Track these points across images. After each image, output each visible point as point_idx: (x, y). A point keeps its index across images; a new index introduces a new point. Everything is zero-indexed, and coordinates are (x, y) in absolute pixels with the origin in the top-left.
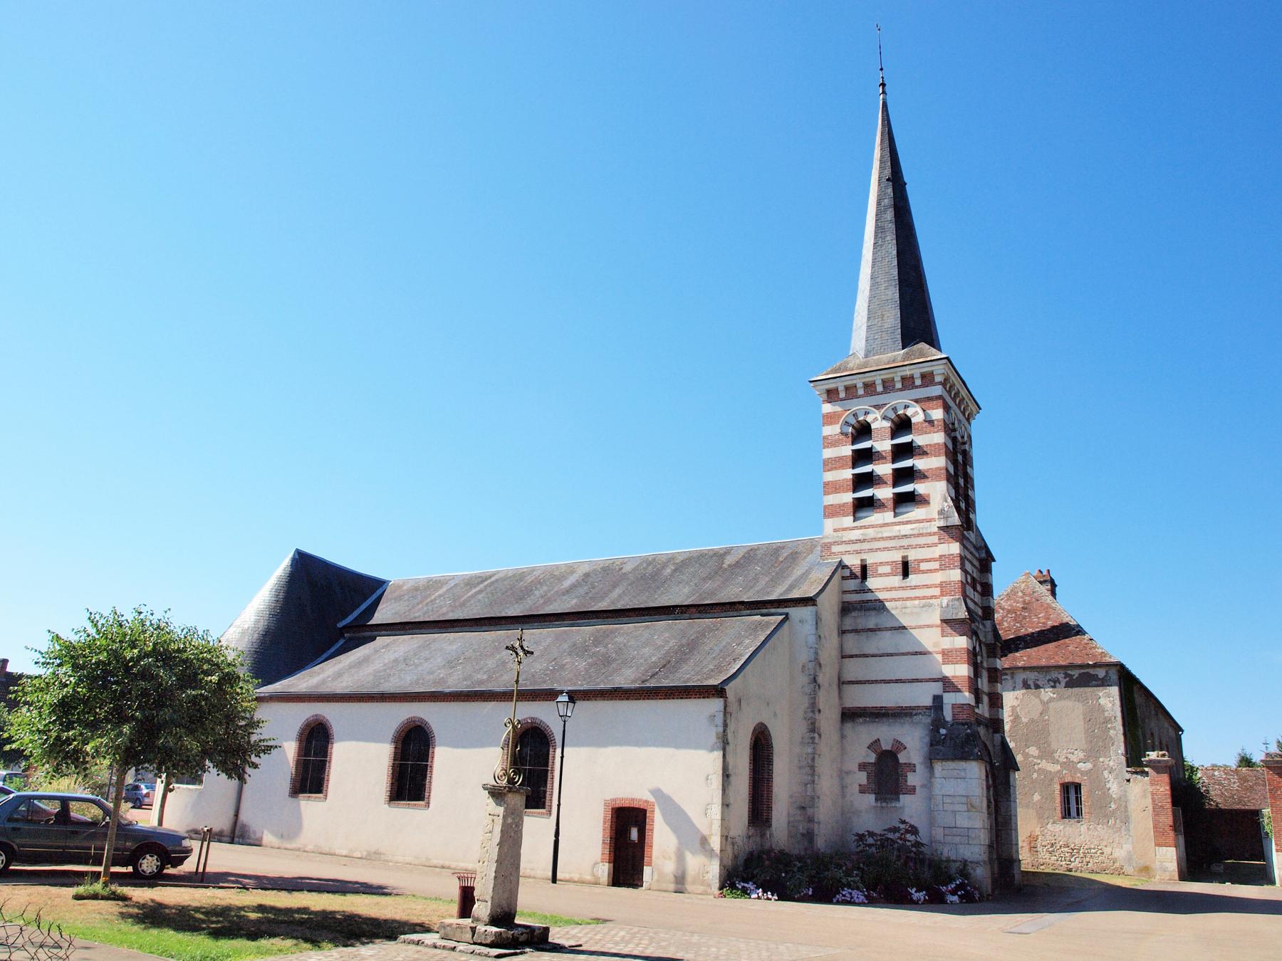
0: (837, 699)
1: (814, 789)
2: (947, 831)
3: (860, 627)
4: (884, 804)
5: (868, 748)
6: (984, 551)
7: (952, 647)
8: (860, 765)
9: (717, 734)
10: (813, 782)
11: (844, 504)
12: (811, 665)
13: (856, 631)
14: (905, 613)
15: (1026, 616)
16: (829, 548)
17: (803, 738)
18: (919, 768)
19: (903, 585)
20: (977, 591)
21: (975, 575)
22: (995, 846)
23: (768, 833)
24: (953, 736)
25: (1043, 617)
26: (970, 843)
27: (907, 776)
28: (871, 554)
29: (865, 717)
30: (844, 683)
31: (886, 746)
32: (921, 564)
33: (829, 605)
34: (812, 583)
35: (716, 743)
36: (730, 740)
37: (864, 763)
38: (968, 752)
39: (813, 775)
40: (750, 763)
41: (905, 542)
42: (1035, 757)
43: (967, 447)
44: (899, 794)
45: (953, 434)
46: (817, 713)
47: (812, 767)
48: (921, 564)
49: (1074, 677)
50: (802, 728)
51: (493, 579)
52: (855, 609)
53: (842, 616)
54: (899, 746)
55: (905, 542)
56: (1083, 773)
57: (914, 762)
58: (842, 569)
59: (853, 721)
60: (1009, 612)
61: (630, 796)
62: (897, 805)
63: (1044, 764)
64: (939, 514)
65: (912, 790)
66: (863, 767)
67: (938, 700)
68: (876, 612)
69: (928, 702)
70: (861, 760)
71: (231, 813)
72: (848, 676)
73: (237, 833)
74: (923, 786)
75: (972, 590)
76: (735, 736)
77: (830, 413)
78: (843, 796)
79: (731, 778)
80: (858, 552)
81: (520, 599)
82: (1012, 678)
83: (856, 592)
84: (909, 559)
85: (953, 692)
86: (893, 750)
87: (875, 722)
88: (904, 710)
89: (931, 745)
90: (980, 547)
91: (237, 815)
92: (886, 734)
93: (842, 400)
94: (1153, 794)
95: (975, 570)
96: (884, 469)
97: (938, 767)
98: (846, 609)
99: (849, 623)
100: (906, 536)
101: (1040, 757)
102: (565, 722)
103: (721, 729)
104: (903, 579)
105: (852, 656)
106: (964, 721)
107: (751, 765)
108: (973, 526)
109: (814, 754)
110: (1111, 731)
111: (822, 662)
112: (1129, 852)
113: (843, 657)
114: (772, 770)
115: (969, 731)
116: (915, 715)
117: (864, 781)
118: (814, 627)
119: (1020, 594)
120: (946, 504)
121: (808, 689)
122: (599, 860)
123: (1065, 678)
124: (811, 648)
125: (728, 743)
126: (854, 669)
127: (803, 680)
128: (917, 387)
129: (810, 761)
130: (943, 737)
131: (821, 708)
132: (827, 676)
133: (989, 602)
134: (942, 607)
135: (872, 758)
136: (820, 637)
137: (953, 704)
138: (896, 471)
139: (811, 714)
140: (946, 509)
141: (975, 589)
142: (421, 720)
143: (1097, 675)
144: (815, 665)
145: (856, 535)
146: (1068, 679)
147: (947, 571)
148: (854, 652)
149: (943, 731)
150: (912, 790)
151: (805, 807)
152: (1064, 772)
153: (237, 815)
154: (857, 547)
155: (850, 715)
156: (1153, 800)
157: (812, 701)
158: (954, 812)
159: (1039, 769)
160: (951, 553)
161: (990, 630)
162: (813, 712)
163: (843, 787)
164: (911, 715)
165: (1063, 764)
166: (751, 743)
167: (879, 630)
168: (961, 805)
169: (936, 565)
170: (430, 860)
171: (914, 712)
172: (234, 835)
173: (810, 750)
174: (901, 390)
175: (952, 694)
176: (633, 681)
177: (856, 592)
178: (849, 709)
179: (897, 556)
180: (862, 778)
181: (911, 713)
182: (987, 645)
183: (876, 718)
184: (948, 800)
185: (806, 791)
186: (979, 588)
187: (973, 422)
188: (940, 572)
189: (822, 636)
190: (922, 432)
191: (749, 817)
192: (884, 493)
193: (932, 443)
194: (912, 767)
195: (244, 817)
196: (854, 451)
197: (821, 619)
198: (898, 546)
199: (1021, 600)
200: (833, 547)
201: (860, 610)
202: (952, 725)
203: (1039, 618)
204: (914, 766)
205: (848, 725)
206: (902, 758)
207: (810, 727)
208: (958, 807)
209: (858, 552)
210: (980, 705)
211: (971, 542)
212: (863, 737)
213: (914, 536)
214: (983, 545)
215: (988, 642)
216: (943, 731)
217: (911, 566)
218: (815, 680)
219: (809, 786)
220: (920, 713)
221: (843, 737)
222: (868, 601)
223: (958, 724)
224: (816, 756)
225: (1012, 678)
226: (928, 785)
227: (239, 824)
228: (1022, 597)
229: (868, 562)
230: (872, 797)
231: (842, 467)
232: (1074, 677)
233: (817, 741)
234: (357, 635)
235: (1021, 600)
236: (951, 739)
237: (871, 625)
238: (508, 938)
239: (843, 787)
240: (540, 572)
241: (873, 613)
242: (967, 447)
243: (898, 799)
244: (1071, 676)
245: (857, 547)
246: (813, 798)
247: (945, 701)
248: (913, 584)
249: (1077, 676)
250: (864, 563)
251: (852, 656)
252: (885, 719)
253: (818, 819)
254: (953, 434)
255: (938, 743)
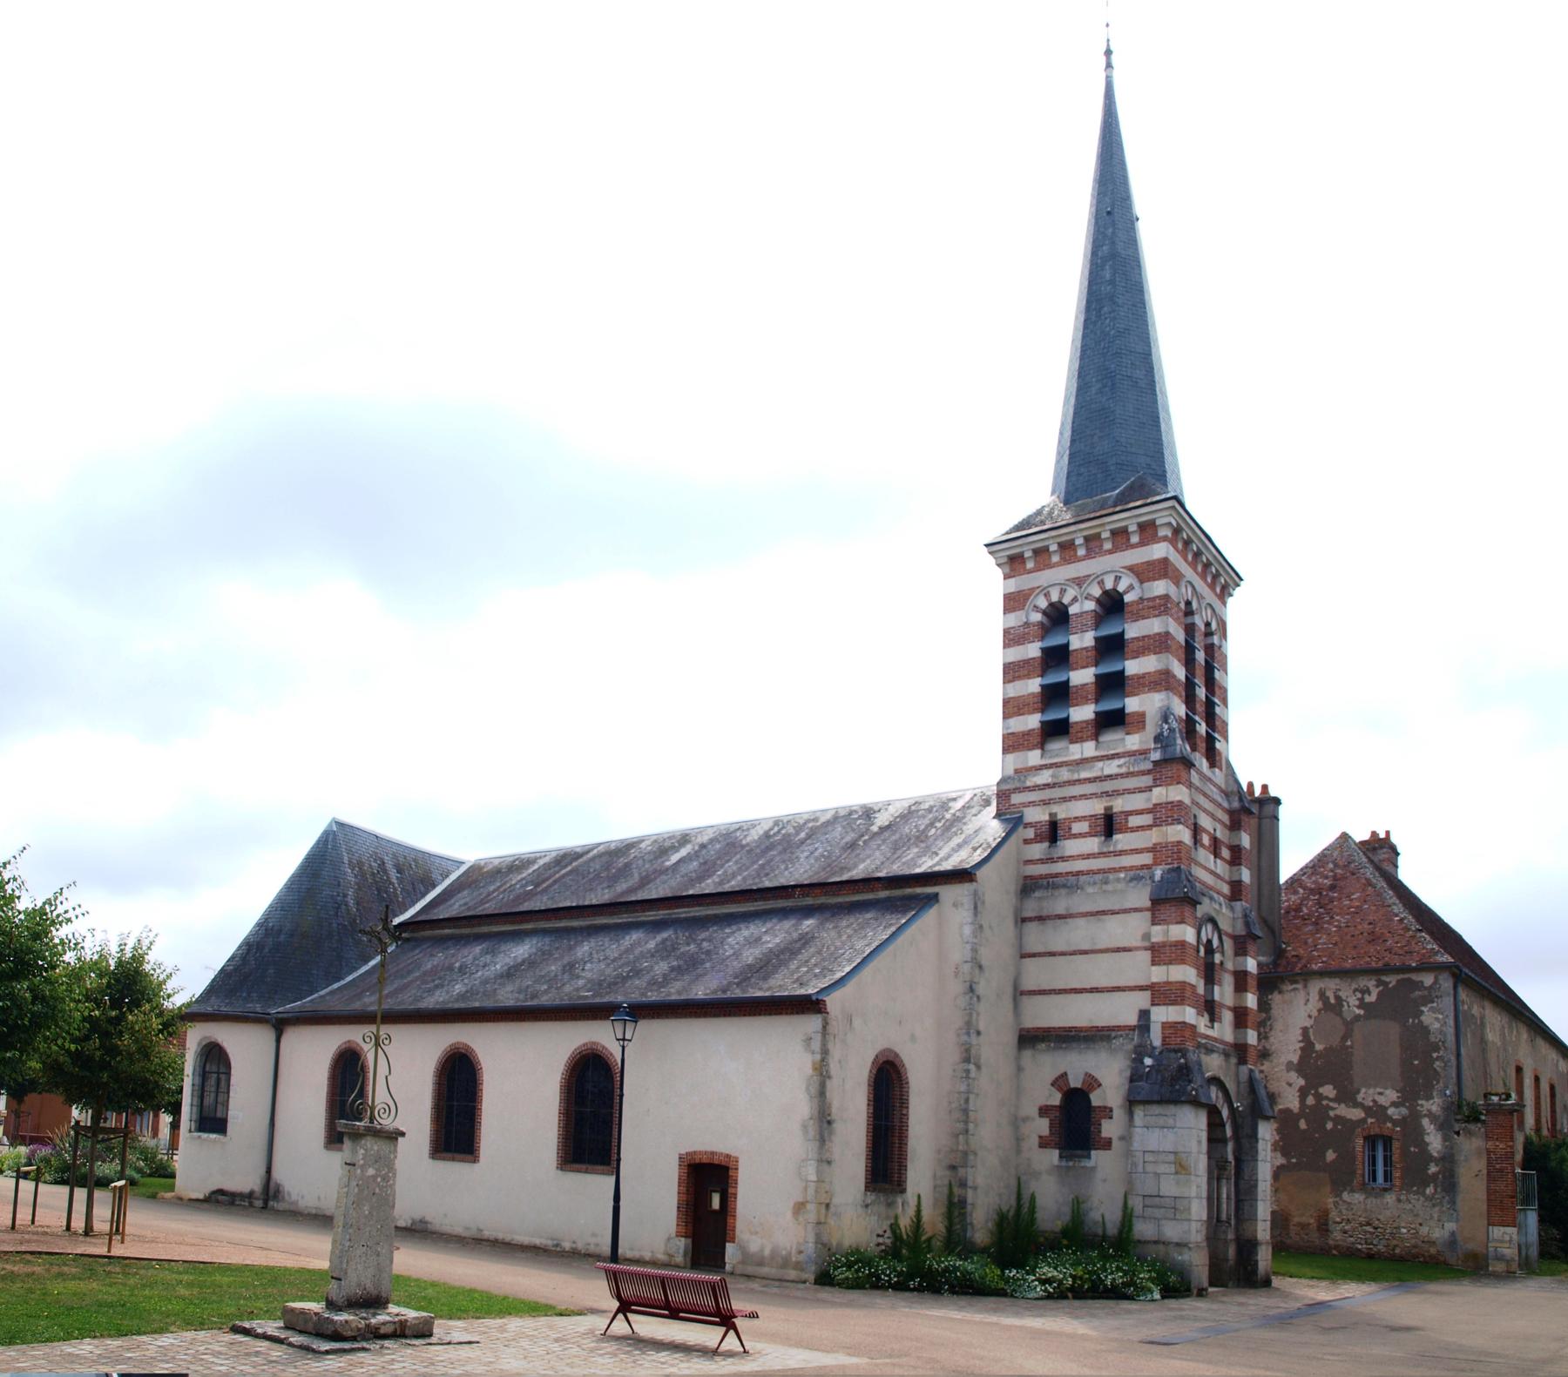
0: (1010, 1015)
1: (967, 1142)
2: (1148, 1201)
3: (1045, 913)
4: (1071, 1164)
5: (1052, 1085)
6: (1237, 798)
7: (1165, 939)
8: (1041, 1109)
9: (814, 1063)
10: (967, 1131)
11: (1030, 731)
12: (966, 968)
13: (1041, 919)
14: (1105, 891)
15: (1334, 897)
16: (1008, 797)
17: (954, 1071)
18: (1118, 1113)
19: (1105, 850)
20: (1223, 859)
21: (1218, 834)
22: (1233, 1222)
23: (900, 1201)
24: (1162, 1068)
25: (1358, 899)
26: (1177, 1217)
27: (1100, 1125)
28: (1064, 806)
29: (1049, 1041)
30: (1023, 993)
31: (1075, 1082)
32: (1130, 818)
33: (997, 885)
34: (975, 849)
35: (812, 1076)
36: (833, 1073)
37: (1047, 1106)
38: (1178, 1091)
39: (966, 1122)
40: (868, 1105)
41: (1108, 786)
42: (1331, 1100)
43: (1216, 639)
44: (1059, 1148)
45: (1189, 620)
46: (973, 1036)
47: (965, 1111)
48: (1130, 818)
49: (1390, 986)
50: (954, 1055)
51: (591, 854)
52: (1040, 887)
53: (1022, 899)
54: (1092, 1083)
55: (1108, 786)
56: (1395, 1123)
57: (1109, 1105)
58: (1025, 828)
59: (1034, 1047)
60: (1312, 891)
61: (709, 1148)
62: (1088, 1165)
63: (1343, 1110)
64: (1155, 742)
65: (1107, 1144)
66: (1044, 1111)
67: (1144, 1015)
68: (1067, 890)
69: (1132, 1020)
70: (1043, 1102)
71: (262, 1171)
72: (1029, 983)
73: (271, 1192)
74: (1122, 1138)
75: (1212, 857)
76: (841, 1067)
77: (1013, 593)
78: (1018, 1151)
79: (834, 1125)
80: (1046, 803)
81: (614, 879)
82: (1305, 987)
83: (1042, 861)
84: (1115, 810)
85: (1164, 1004)
86: (1084, 1088)
87: (1061, 1048)
88: (1099, 1031)
89: (1132, 1080)
90: (1232, 792)
91: (269, 1171)
92: (1077, 1064)
93: (1030, 572)
94: (1489, 1152)
95: (1219, 827)
96: (1082, 677)
97: (1139, 1113)
98: (1028, 886)
99: (1030, 909)
100: (1110, 777)
101: (1338, 1100)
102: (623, 1047)
103: (818, 1057)
104: (1105, 840)
105: (1033, 955)
106: (1176, 1047)
107: (872, 1108)
108: (1221, 760)
109: (969, 1092)
110: (1438, 1063)
111: (983, 963)
112: (1453, 1234)
113: (1023, 956)
114: (907, 1115)
115: (1182, 1061)
116: (1114, 1038)
117: (1046, 1131)
118: (972, 911)
119: (1331, 866)
120: (1166, 727)
121: (963, 1002)
122: (674, 1235)
123: (1377, 986)
124: (967, 943)
125: (829, 1077)
126: (1036, 974)
127: (956, 987)
128: (1133, 546)
129: (962, 1102)
130: (1147, 1069)
131: (981, 1027)
132: (993, 984)
133: (1240, 874)
134: (1154, 882)
135: (1056, 1099)
136: (981, 927)
137: (1163, 1023)
138: (1100, 678)
139: (965, 1038)
140: (1165, 734)
141: (1216, 854)
142: (468, 1047)
143: (1422, 982)
144: (972, 968)
145: (1045, 777)
146: (1381, 988)
147: (1164, 828)
148: (1040, 949)
149: (1148, 1061)
150: (1107, 1144)
151: (956, 1166)
152: (1370, 1120)
153: (269, 1171)
154: (1046, 794)
155: (1029, 1039)
156: (1489, 1163)
157: (967, 1018)
158: (1157, 1175)
159: (1337, 1116)
160: (1170, 800)
161: (1240, 915)
162: (968, 1034)
163: (1019, 1140)
164: (1108, 1039)
165: (1368, 1110)
166: (870, 1076)
167: (1071, 916)
168: (1166, 1165)
169: (1146, 819)
170: (482, 1231)
171: (1113, 1034)
172: (267, 1194)
173: (963, 1088)
174: (1110, 552)
175: (1163, 1008)
176: (715, 992)
177: (1042, 861)
178: (1028, 1030)
179: (1097, 807)
180: (1043, 1126)
181: (1109, 1036)
182: (1235, 938)
183: (1064, 1042)
184: (1149, 1157)
185: (958, 1144)
186: (1226, 853)
187: (1230, 601)
188: (1154, 829)
189: (986, 926)
190: (1139, 616)
191: (866, 1179)
192: (1082, 713)
193: (1151, 633)
194: (1107, 1112)
195: (279, 1174)
196: (1043, 650)
197: (983, 903)
198: (1099, 792)
199: (1331, 874)
200: (1013, 795)
201: (1047, 887)
202: (1161, 1053)
203: (1351, 900)
204: (1111, 1110)
205: (1027, 1054)
206: (1096, 1099)
207: (964, 1055)
208: (1162, 1168)
209: (1046, 803)
210: (1216, 1025)
211: (1215, 785)
212: (1045, 1067)
213: (1121, 776)
214: (1235, 789)
215: (1237, 933)
216: (1148, 1061)
217: (1117, 819)
218: (971, 990)
219: (961, 1137)
220: (1121, 1036)
221: (1020, 1069)
222: (1057, 875)
223: (1170, 1051)
224: (972, 1097)
225: (1305, 987)
226: (1126, 1138)
227: (272, 1184)
228: (1332, 871)
229: (1059, 817)
230: (1056, 1153)
231: (1028, 676)
232: (1390, 986)
233: (973, 1075)
234: (416, 935)
235: (1331, 874)
236: (1158, 1071)
237: (1061, 910)
238: (359, 1329)
239: (1019, 1140)
240: (648, 842)
241: (1063, 891)
242: (1216, 639)
243: (1089, 1157)
244: (1386, 984)
245: (1046, 794)
246: (965, 1154)
247: (1153, 1017)
248: (1119, 847)
249: (1394, 983)
250: (1054, 819)
251: (1033, 955)
252: (1074, 1045)
253: (974, 1182)
254: (1189, 620)
255: (1140, 1078)
